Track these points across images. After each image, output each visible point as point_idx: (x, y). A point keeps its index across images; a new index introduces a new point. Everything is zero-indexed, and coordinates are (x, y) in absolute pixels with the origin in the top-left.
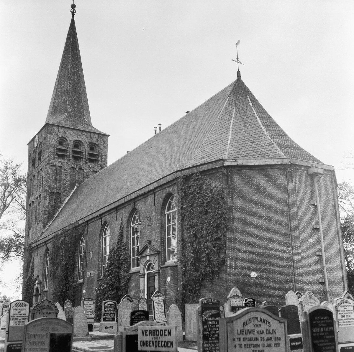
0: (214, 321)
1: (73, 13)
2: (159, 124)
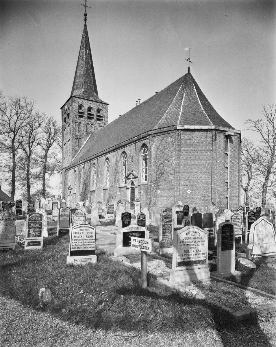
0: (168, 224)
1: (86, 20)
2: (139, 100)
